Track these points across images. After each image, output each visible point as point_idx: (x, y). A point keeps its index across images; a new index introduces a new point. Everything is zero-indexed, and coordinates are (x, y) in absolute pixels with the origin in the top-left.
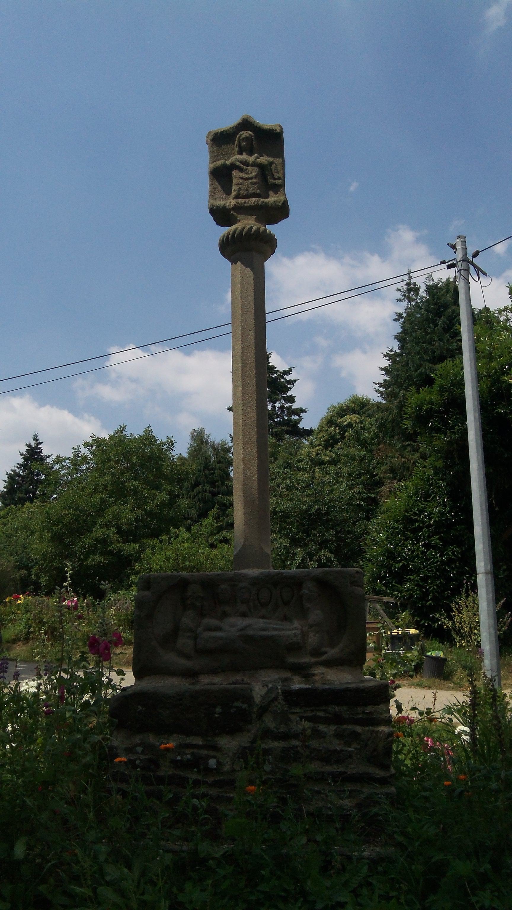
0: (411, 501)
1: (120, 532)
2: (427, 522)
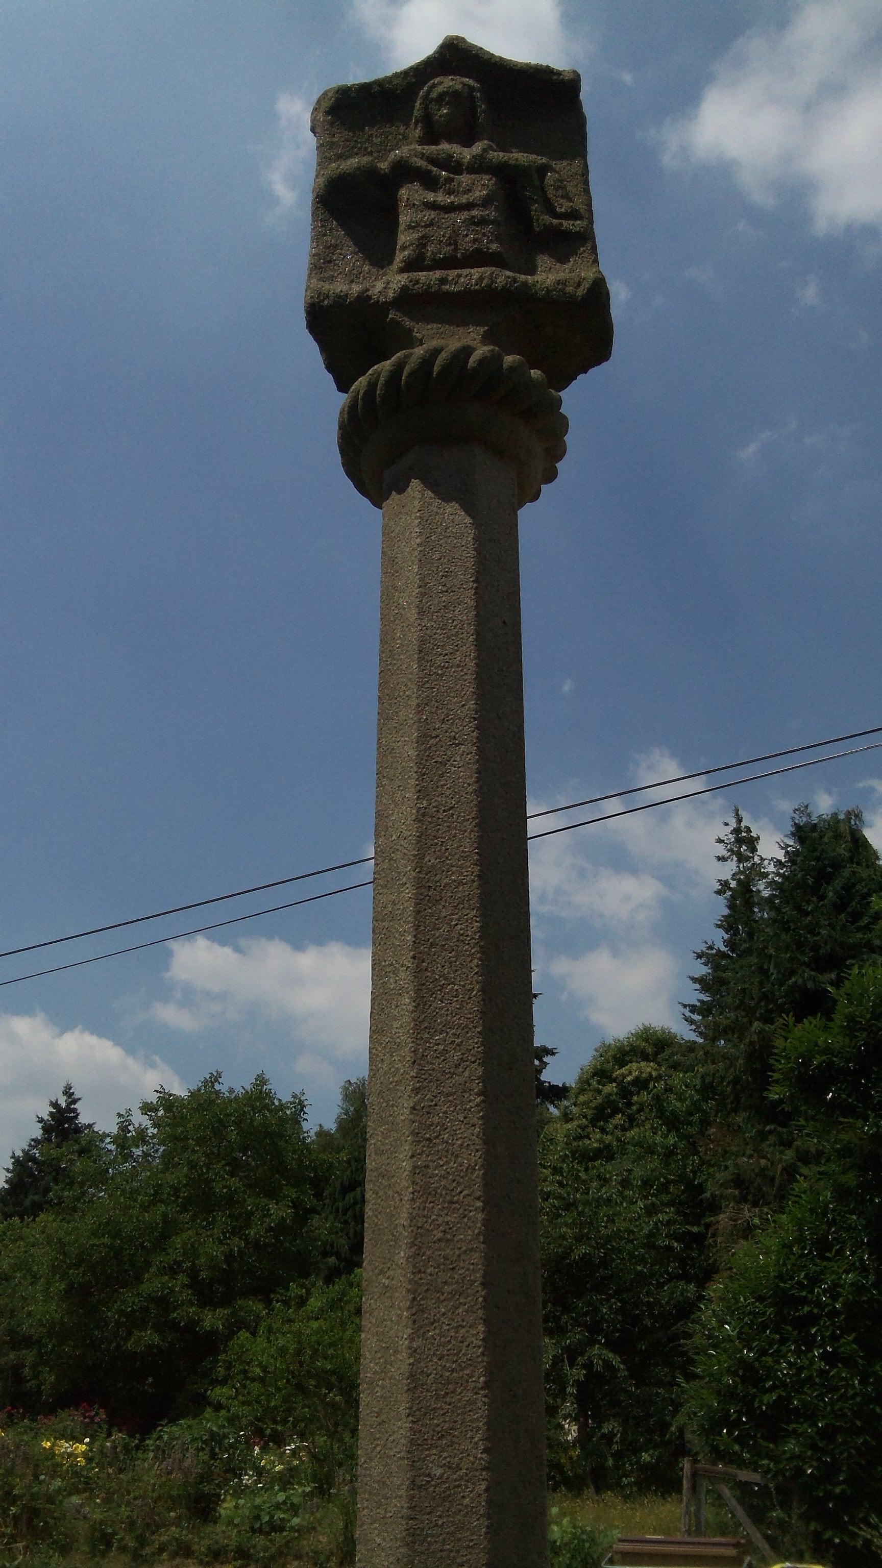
0: (791, 1256)
1: (195, 1283)
2: (827, 1305)
